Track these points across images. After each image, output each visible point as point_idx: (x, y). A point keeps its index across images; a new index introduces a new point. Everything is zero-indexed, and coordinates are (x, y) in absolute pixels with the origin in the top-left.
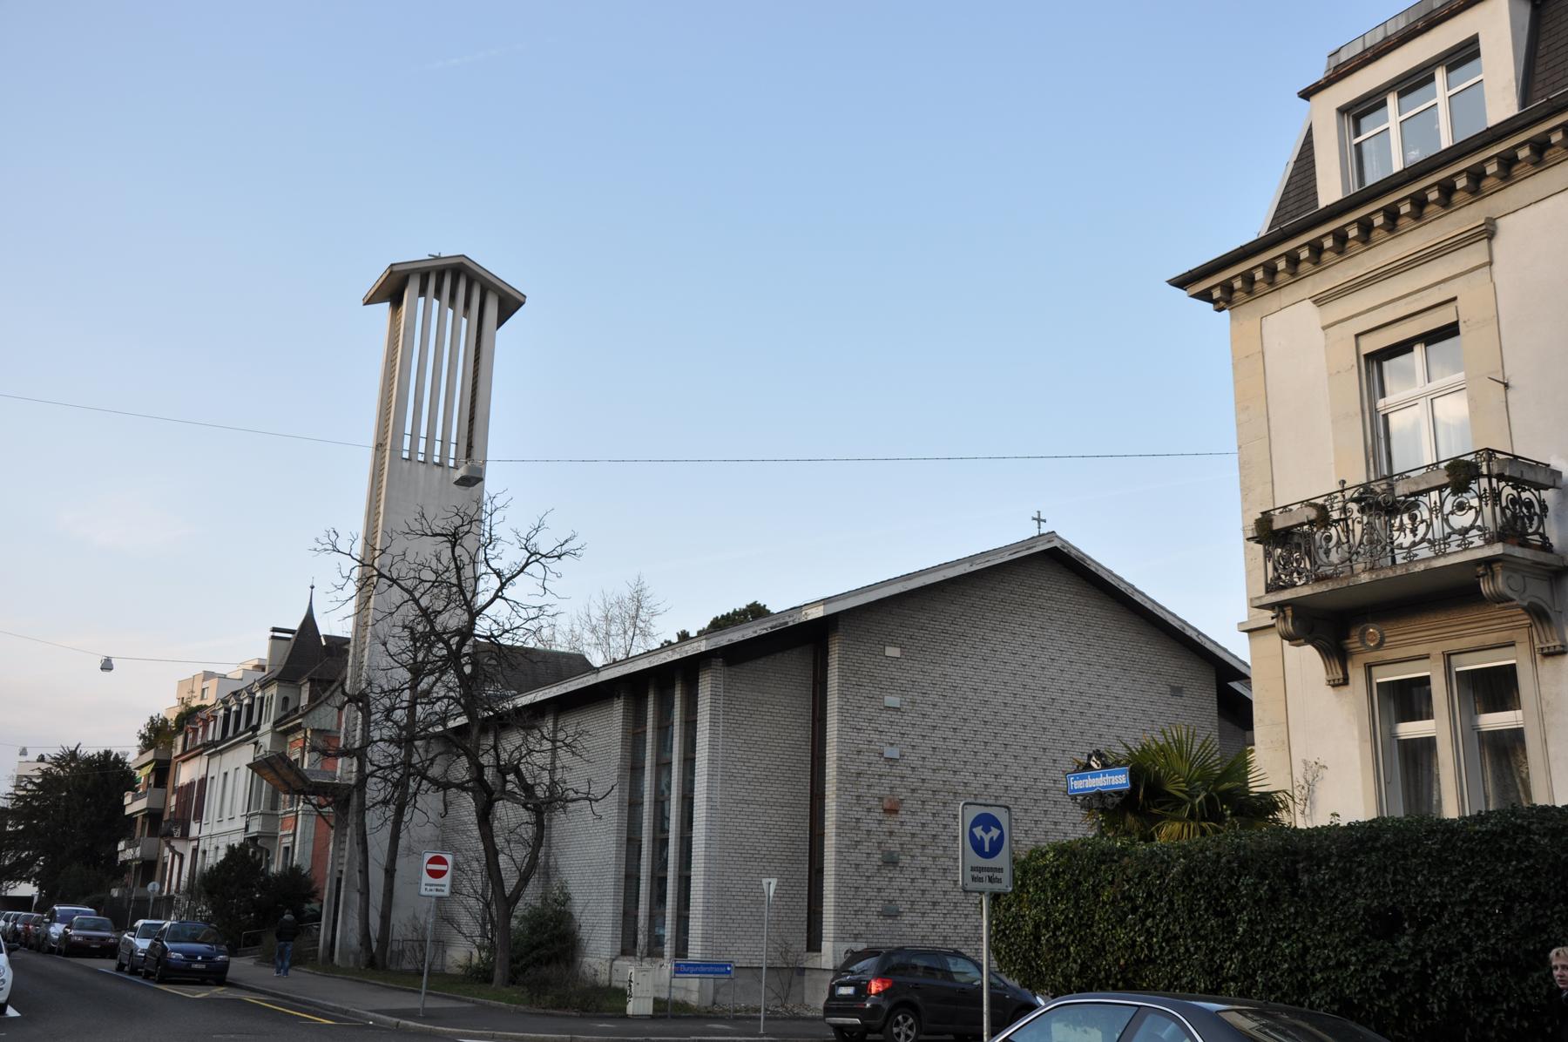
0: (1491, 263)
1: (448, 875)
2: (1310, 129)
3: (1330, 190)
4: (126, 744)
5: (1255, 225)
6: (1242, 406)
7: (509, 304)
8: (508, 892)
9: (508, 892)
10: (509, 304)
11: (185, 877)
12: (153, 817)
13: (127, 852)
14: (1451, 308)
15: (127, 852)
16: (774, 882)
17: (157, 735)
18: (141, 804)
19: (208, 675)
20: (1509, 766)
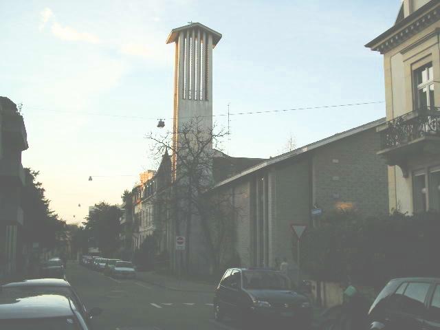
0: (438, 42)
1: (184, 243)
2: (403, 5)
3: (407, 14)
4: (117, 201)
5: (391, 23)
6: (386, 71)
7: (216, 38)
8: (304, 227)
9: (304, 227)
10: (216, 38)
11: (139, 244)
12: (128, 224)
13: (122, 237)
14: (430, 57)
15: (122, 237)
16: (58, 302)
17: (127, 197)
18: (124, 221)
19: (149, 171)
20: (182, 132)
